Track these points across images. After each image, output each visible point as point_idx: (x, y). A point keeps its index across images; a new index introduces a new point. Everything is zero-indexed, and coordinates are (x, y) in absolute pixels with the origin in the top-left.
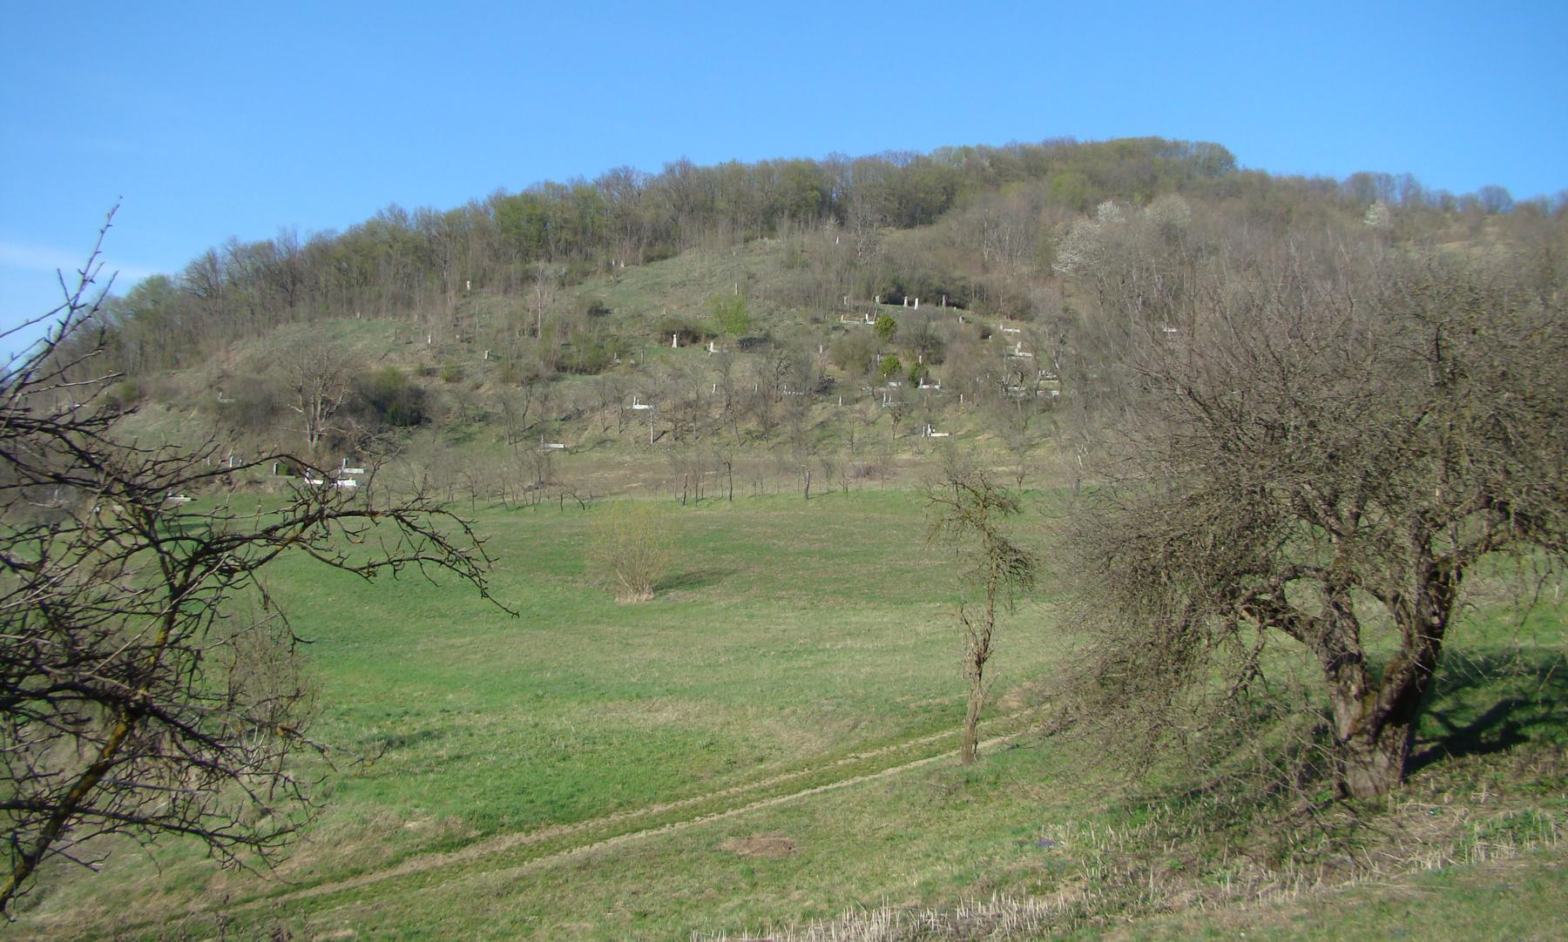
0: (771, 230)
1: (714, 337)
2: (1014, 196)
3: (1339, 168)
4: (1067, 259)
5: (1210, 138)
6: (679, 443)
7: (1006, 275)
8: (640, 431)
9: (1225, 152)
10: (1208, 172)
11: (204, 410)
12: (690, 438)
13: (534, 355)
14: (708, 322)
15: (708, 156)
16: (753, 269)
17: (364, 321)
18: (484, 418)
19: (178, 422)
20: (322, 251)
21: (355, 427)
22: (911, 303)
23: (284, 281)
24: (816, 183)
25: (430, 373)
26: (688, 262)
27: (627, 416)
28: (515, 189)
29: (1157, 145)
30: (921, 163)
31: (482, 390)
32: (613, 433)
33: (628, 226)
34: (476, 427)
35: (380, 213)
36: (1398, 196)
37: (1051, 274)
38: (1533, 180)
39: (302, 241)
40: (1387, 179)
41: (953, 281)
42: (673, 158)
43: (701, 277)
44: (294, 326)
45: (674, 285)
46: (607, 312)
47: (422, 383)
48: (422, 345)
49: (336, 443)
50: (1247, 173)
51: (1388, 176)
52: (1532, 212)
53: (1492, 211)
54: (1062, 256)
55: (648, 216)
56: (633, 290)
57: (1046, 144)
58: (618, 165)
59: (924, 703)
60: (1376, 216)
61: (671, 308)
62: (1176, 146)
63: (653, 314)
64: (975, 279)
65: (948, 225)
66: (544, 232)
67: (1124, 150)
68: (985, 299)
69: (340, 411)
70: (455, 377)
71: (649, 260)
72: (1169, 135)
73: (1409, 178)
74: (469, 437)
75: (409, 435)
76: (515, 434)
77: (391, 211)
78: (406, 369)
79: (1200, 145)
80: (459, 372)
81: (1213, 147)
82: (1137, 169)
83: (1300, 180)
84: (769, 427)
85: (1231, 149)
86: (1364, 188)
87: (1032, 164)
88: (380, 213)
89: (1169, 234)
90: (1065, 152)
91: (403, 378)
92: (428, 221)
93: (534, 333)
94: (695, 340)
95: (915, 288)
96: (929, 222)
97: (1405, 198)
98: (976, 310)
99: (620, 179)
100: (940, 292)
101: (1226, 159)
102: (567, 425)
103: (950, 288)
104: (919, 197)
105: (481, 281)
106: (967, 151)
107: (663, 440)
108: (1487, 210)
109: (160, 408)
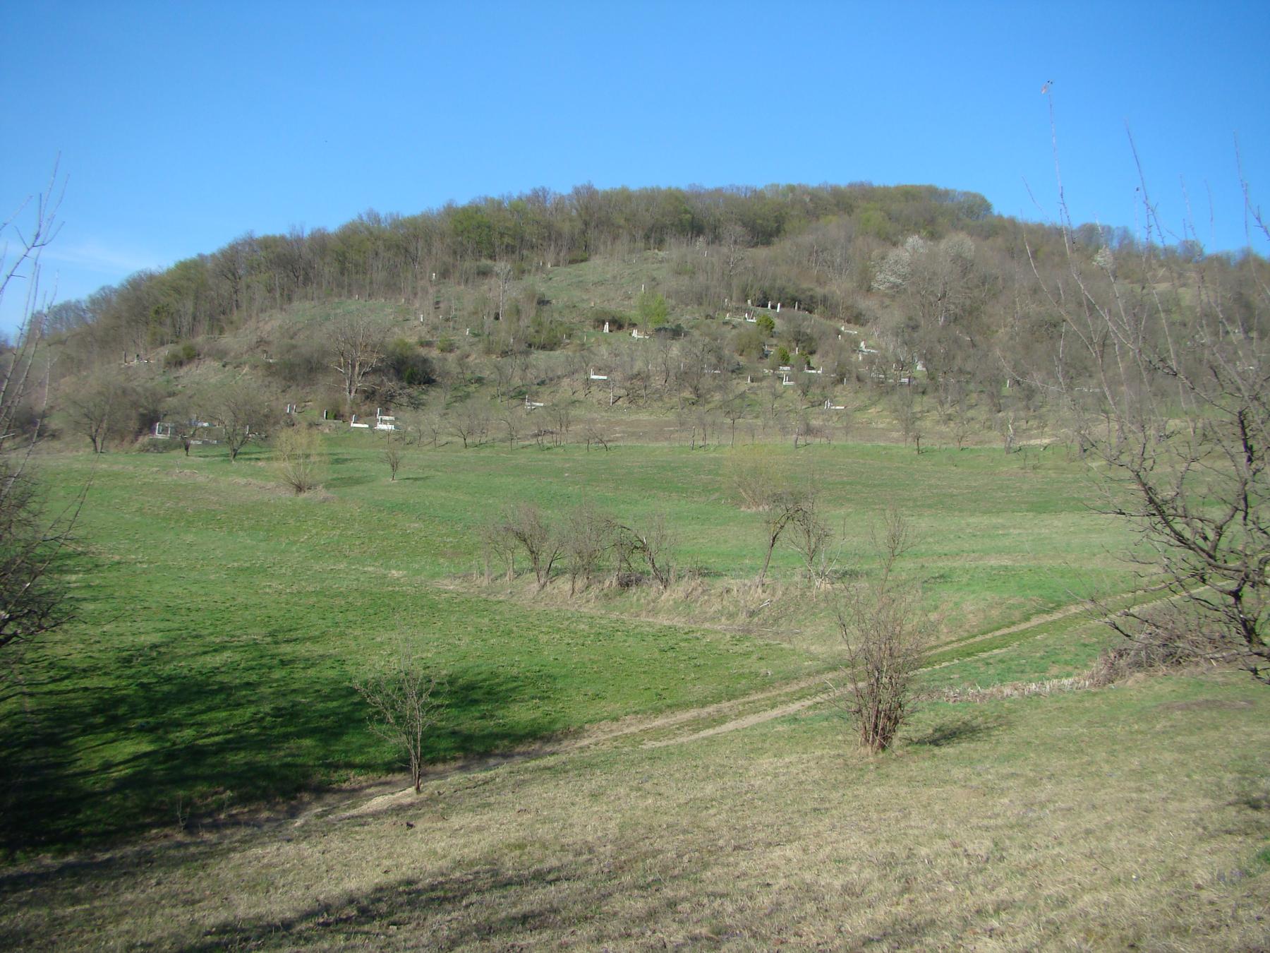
0: (660, 243)
1: (634, 325)
2: (833, 226)
3: (1076, 218)
4: (883, 279)
5: (973, 189)
6: (634, 406)
7: (839, 287)
8: (601, 395)
9: (983, 200)
10: (972, 214)
11: (255, 367)
12: (641, 402)
13: (504, 333)
14: (634, 314)
15: (605, 183)
16: (655, 274)
17: (362, 301)
18: (480, 380)
19: (234, 377)
20: (320, 243)
21: (391, 385)
22: (774, 307)
23: (288, 266)
24: (688, 208)
25: (428, 344)
26: (596, 267)
27: (588, 383)
28: (462, 201)
29: (932, 192)
30: (758, 196)
31: (471, 358)
32: (580, 395)
33: (550, 235)
34: (472, 388)
35: (361, 217)
36: (1115, 244)
37: (869, 289)
38: (1222, 238)
39: (307, 233)
40: (1108, 230)
41: (804, 291)
42: (581, 182)
43: (612, 277)
44: (308, 304)
45: (594, 284)
46: (548, 302)
47: (423, 351)
48: (416, 323)
49: (369, 395)
50: (1000, 217)
51: (1109, 228)
52: (1220, 262)
53: (1188, 261)
54: (880, 277)
55: (566, 228)
56: (559, 282)
57: (850, 186)
58: (538, 186)
59: (1032, 563)
60: (1103, 259)
61: (595, 302)
62: (946, 194)
63: (585, 305)
64: (819, 291)
65: (782, 247)
66: (487, 238)
67: (909, 194)
68: (829, 306)
69: (375, 371)
70: (449, 348)
71: (573, 262)
72: (941, 184)
73: (1125, 231)
74: (468, 396)
75: (425, 392)
76: (503, 394)
77: (369, 215)
78: (412, 340)
79: (966, 194)
80: (451, 345)
81: (975, 196)
82: (925, 211)
83: (1041, 226)
84: (700, 397)
85: (989, 199)
86: (1090, 238)
87: (842, 202)
88: (361, 217)
89: (965, 266)
90: (867, 193)
91: (411, 348)
92: (398, 224)
93: (497, 318)
94: (620, 327)
95: (775, 295)
96: (768, 243)
97: (1120, 244)
98: (822, 314)
99: (538, 197)
100: (794, 300)
101: (986, 207)
102: (542, 389)
103: (802, 297)
104: (764, 222)
105: (445, 274)
106: (792, 189)
107: (619, 403)
108: (1186, 261)
109: (218, 364)
